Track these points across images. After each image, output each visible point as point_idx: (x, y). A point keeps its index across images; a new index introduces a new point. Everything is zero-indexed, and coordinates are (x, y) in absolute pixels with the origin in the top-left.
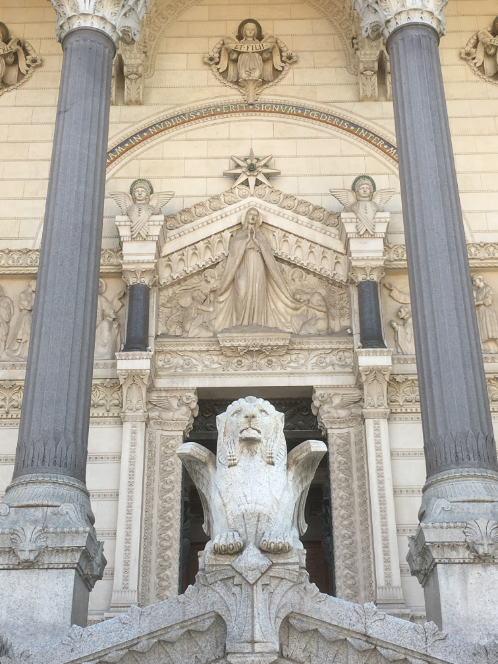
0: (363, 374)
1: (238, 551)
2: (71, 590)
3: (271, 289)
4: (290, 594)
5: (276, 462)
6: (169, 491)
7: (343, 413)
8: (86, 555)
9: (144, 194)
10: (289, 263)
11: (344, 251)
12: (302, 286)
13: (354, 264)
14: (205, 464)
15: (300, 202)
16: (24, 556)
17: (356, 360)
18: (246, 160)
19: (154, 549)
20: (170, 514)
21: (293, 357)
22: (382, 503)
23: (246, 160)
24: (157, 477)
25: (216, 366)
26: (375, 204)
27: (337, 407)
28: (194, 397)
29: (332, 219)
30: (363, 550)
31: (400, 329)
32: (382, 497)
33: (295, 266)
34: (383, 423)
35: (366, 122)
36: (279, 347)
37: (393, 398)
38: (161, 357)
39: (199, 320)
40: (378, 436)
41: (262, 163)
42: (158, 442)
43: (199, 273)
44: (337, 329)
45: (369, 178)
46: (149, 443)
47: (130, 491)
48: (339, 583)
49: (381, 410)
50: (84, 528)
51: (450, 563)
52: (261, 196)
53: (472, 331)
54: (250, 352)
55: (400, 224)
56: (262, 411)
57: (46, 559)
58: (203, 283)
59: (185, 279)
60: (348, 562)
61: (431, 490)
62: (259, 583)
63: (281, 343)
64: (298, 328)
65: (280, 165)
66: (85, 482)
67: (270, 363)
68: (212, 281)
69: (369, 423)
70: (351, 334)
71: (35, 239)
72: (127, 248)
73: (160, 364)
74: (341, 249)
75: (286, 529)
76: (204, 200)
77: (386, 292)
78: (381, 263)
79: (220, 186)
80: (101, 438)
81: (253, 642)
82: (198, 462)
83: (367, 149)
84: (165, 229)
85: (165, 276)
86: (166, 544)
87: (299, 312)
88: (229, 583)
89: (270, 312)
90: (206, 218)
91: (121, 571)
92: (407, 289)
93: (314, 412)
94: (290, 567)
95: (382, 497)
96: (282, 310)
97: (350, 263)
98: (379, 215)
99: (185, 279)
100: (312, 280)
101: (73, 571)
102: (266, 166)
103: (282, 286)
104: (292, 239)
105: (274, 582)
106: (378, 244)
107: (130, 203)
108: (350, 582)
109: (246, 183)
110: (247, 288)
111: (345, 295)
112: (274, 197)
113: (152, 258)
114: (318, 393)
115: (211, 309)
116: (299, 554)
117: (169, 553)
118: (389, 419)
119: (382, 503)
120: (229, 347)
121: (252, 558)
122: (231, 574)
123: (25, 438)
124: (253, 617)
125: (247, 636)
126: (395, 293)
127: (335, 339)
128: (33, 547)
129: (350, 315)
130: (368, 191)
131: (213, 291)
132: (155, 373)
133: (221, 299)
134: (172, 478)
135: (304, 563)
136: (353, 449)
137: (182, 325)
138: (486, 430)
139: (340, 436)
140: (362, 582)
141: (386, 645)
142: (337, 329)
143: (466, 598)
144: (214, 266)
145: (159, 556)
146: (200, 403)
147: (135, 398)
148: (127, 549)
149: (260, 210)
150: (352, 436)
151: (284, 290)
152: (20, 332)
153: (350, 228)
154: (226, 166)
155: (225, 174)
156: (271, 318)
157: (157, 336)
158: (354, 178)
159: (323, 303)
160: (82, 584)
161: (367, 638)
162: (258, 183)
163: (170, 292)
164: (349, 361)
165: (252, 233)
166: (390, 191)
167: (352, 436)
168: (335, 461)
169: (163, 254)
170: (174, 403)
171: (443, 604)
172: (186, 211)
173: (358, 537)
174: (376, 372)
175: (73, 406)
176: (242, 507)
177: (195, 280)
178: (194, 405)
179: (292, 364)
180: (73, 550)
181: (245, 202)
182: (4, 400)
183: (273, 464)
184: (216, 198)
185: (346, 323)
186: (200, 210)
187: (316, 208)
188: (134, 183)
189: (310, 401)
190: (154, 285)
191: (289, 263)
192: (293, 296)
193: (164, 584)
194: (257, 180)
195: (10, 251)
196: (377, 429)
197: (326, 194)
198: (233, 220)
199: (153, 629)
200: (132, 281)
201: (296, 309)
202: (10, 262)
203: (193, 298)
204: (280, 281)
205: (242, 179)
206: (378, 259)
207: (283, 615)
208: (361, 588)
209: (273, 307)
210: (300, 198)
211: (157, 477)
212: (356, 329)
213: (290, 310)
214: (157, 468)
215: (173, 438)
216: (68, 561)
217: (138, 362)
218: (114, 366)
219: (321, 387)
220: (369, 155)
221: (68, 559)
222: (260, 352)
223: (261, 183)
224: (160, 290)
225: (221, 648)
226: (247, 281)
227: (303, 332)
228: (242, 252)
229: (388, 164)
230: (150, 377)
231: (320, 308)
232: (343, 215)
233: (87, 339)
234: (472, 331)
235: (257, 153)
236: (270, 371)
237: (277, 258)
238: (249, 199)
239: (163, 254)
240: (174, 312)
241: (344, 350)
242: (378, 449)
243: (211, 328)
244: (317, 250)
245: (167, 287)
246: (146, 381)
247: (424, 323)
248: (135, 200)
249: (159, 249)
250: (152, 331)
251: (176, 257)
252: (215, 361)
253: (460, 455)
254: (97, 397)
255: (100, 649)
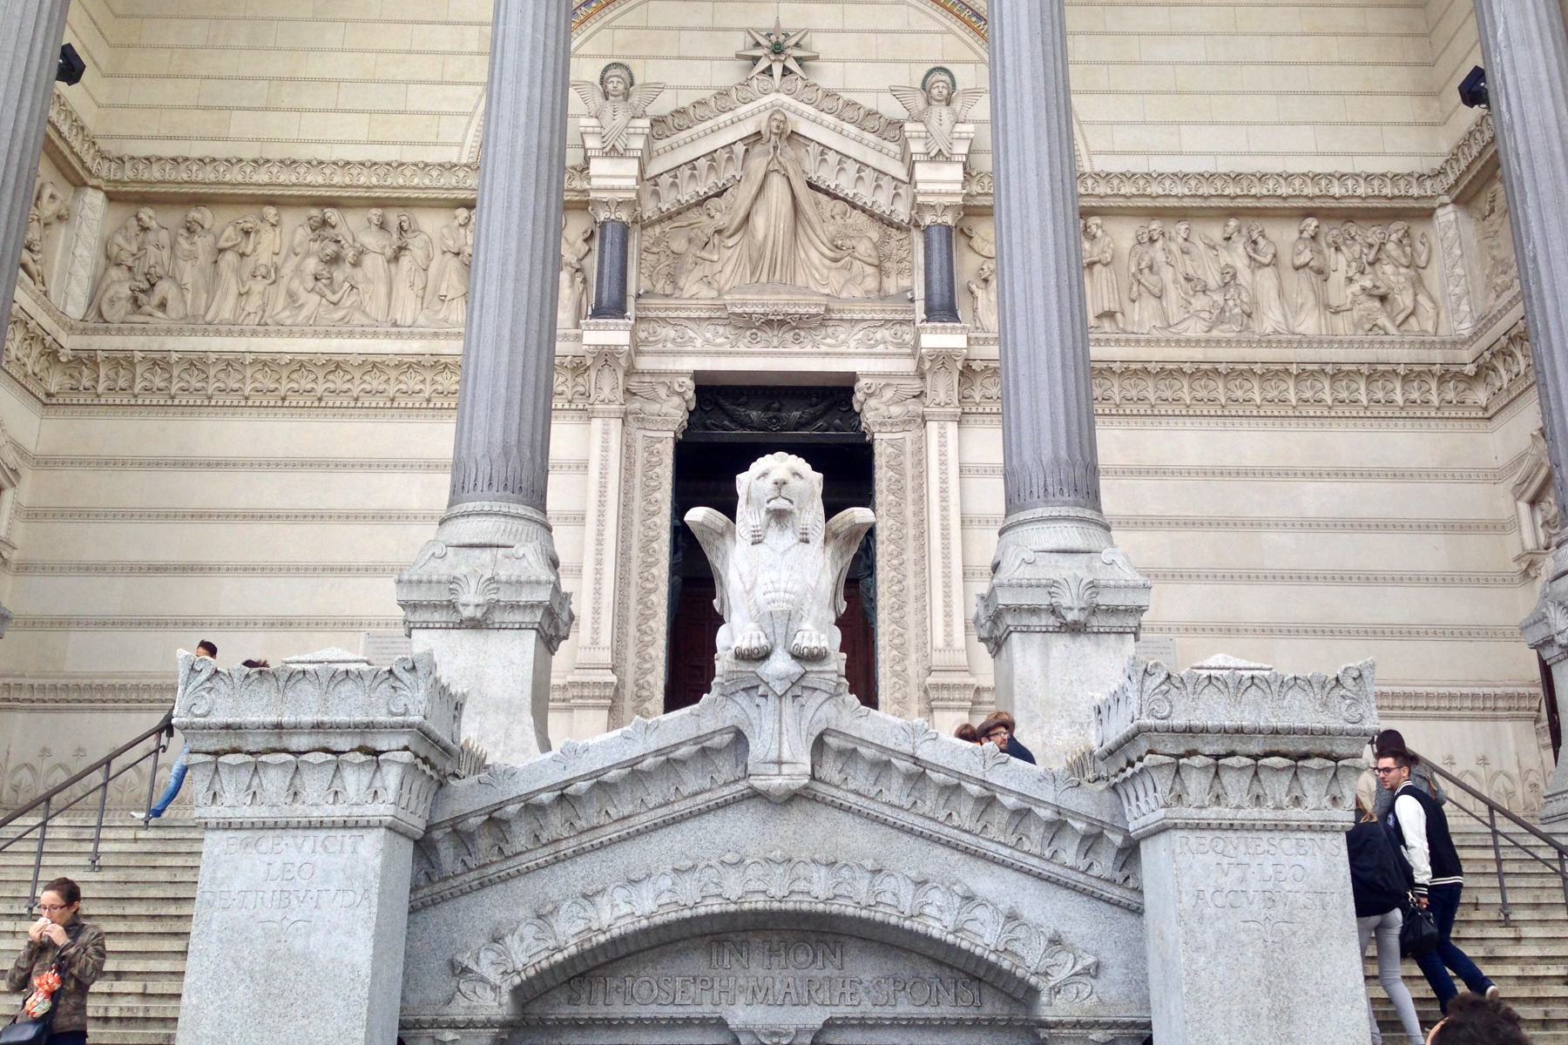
0: (926, 360)
1: (763, 656)
2: (531, 657)
3: (800, 230)
4: (825, 706)
5: (810, 537)
6: (654, 514)
7: (896, 410)
8: (550, 612)
9: (621, 87)
10: (827, 193)
11: (906, 179)
12: (845, 226)
13: (920, 199)
14: (722, 535)
15: (848, 104)
16: (467, 613)
17: (917, 340)
18: (769, 35)
19: (633, 593)
20: (655, 545)
21: (830, 330)
22: (945, 537)
23: (769, 35)
24: (637, 494)
25: (721, 340)
26: (954, 112)
27: (888, 404)
28: (690, 384)
29: (892, 129)
30: (917, 599)
31: (979, 293)
32: (945, 528)
33: (836, 197)
34: (952, 428)
35: (953, 27)
36: (811, 316)
37: (966, 393)
38: (643, 326)
39: (698, 273)
40: (943, 445)
41: (793, 41)
42: (639, 445)
43: (700, 203)
44: (893, 291)
45: (946, 71)
46: (627, 447)
47: (601, 514)
48: (881, 698)
49: (949, 410)
50: (545, 574)
51: (1028, 630)
52: (789, 93)
53: (1077, 318)
54: (769, 323)
55: (986, 142)
56: (795, 474)
57: (497, 617)
58: (705, 218)
59: (679, 213)
60: (896, 615)
61: (1009, 535)
62: (789, 695)
63: (813, 311)
64: (838, 287)
65: (819, 44)
66: (545, 512)
67: (797, 339)
68: (718, 216)
69: (932, 427)
70: (912, 300)
71: (461, 145)
72: (597, 167)
73: (642, 335)
74: (903, 175)
75: (819, 632)
76: (707, 94)
77: (963, 240)
78: (959, 200)
79: (728, 75)
80: (565, 438)
81: (780, 763)
82: (713, 532)
83: (948, 23)
84: (651, 138)
85: (649, 210)
86: (649, 586)
87: (839, 264)
88: (753, 692)
89: (799, 263)
90: (709, 124)
91: (590, 620)
92: (992, 237)
93: (857, 408)
94: (827, 676)
95: (945, 528)
96: (817, 262)
97: (915, 197)
98: (959, 127)
99: (679, 213)
100: (858, 218)
101: (534, 633)
102: (797, 45)
103: (818, 227)
104: (832, 158)
105: (806, 693)
106: (956, 172)
107: (599, 99)
108: (897, 641)
109: (768, 71)
110: (767, 228)
111: (906, 242)
112: (808, 94)
113: (632, 183)
114: (861, 384)
115: (715, 258)
116: (838, 661)
117: (653, 597)
118: (959, 422)
119: (945, 537)
120: (740, 315)
121: (780, 665)
122: (755, 683)
123: (464, 453)
124: (780, 733)
125: (773, 755)
126: (977, 243)
127: (889, 306)
128: (480, 600)
129: (911, 270)
130: (945, 92)
131: (719, 232)
132: (637, 349)
133: (730, 242)
134: (658, 495)
135: (843, 671)
136: (908, 462)
137: (673, 279)
138: (1087, 454)
139: (891, 443)
140: (913, 642)
141: (937, 768)
142: (893, 291)
143: (1047, 677)
144: (719, 195)
145: (640, 601)
146: (699, 390)
147: (607, 386)
148: (597, 592)
149: (788, 114)
150: (908, 443)
151: (819, 232)
152: (444, 286)
153: (916, 147)
154: (739, 43)
155: (738, 56)
156: (800, 271)
157: (639, 296)
158: (932, 66)
159: (874, 253)
160: (542, 647)
161: (916, 760)
162: (786, 71)
163: (657, 229)
164: (907, 338)
165: (775, 148)
166: (976, 92)
167: (908, 443)
168: (881, 535)
169: (647, 176)
170: (663, 392)
171: (1016, 683)
172: (681, 112)
173: (910, 581)
174: (943, 358)
175: (529, 409)
176: (768, 596)
177: (693, 216)
178: (690, 394)
179: (829, 341)
180: (533, 606)
181: (766, 100)
182: (423, 381)
183: (807, 541)
184: (723, 94)
185: (905, 282)
186: (700, 111)
187: (870, 114)
188: (606, 70)
189: (850, 391)
190: (635, 222)
191: (827, 193)
192: (832, 241)
193: (647, 639)
194: (785, 68)
195: (426, 165)
196: (942, 436)
197: (884, 91)
198: (748, 129)
199: (662, 745)
200: (603, 215)
201: (836, 260)
202: (427, 182)
203: (690, 241)
204: (814, 220)
205: (763, 65)
206: (954, 194)
207: (816, 733)
208: (912, 649)
209: (803, 256)
210: (846, 96)
211: (637, 494)
212: (920, 293)
213: (827, 262)
214: (637, 482)
215: (660, 440)
216: (527, 619)
217: (614, 335)
218: (579, 338)
219: (867, 375)
220: (949, 31)
221: (527, 617)
222: (782, 323)
223: (791, 72)
224: (643, 228)
225: (742, 767)
226: (768, 219)
227: (844, 295)
228: (760, 175)
229: (976, 46)
230: (629, 355)
231: (870, 260)
232: (908, 127)
233: (547, 313)
234: (1077, 318)
235: (786, 24)
236: (796, 349)
237: (811, 185)
238: (772, 97)
239: (647, 176)
240: (663, 258)
241: (901, 322)
242: (943, 463)
243: (715, 285)
244: (868, 174)
245: (652, 224)
246: (623, 362)
247: (1013, 304)
248: (606, 95)
249: (642, 171)
250: (632, 289)
251: (666, 180)
252: (720, 336)
253: (1050, 489)
254: (561, 383)
255: (599, 767)
